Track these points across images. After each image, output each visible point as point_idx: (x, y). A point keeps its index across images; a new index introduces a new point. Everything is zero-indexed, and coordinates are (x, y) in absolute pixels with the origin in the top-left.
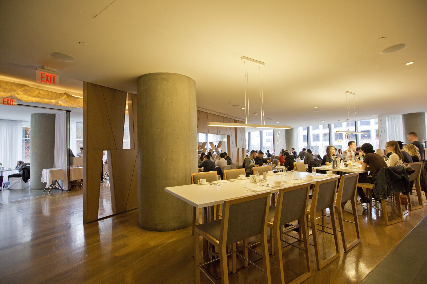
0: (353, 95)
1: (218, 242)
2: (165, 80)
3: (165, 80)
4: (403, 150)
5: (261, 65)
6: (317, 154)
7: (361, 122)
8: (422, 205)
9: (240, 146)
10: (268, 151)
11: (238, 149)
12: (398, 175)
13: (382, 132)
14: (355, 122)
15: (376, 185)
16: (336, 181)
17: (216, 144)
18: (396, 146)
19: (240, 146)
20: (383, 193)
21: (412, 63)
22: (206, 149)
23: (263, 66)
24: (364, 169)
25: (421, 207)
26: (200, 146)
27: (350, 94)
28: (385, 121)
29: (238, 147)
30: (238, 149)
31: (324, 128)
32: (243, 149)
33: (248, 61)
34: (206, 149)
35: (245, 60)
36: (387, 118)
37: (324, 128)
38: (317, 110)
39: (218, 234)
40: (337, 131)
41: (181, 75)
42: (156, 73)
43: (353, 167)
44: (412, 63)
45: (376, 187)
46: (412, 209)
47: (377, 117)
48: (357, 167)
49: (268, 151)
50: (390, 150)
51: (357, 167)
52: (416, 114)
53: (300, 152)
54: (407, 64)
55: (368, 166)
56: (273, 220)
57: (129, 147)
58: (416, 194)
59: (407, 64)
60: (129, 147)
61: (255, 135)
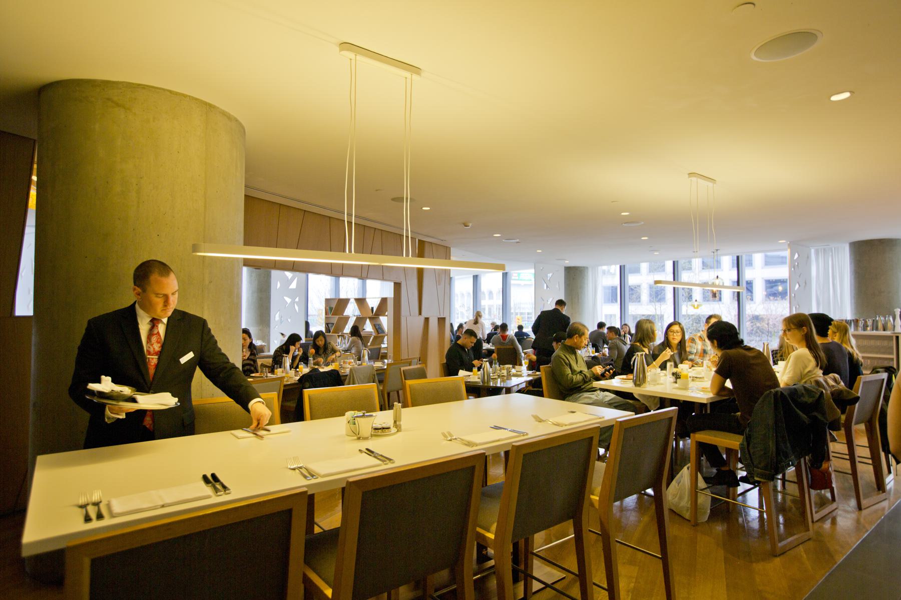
0: (710, 184)
1: (329, 592)
2: (118, 105)
3: (118, 105)
4: (829, 339)
5: (407, 74)
6: (781, 327)
7: (766, 256)
8: (884, 491)
9: (431, 311)
10: (520, 327)
11: (427, 319)
12: (801, 413)
13: (770, 292)
14: (738, 257)
15: (748, 439)
16: (671, 418)
17: (373, 303)
18: (812, 327)
19: (431, 311)
20: (762, 465)
21: (846, 95)
22: (347, 318)
23: (415, 77)
24: (715, 391)
25: (883, 496)
26: (331, 309)
27: (701, 182)
28: (808, 257)
29: (425, 314)
30: (427, 319)
31: (690, 269)
32: (442, 321)
33: (359, 58)
34: (347, 318)
35: (351, 55)
36: (813, 251)
37: (690, 269)
38: (628, 221)
39: (330, 569)
40: (656, 282)
41: (177, 94)
42: (82, 80)
43: (691, 384)
44: (846, 95)
45: (748, 445)
46: (864, 502)
47: (787, 247)
48: (699, 382)
49: (520, 327)
50: (792, 340)
51: (699, 382)
52: (881, 242)
53: (592, 333)
54: (834, 98)
55: (728, 384)
56: (494, 527)
57: (30, 312)
58: (870, 461)
59: (834, 98)
60: (30, 312)
61: (462, 285)
